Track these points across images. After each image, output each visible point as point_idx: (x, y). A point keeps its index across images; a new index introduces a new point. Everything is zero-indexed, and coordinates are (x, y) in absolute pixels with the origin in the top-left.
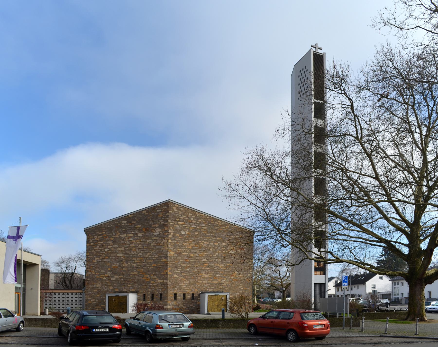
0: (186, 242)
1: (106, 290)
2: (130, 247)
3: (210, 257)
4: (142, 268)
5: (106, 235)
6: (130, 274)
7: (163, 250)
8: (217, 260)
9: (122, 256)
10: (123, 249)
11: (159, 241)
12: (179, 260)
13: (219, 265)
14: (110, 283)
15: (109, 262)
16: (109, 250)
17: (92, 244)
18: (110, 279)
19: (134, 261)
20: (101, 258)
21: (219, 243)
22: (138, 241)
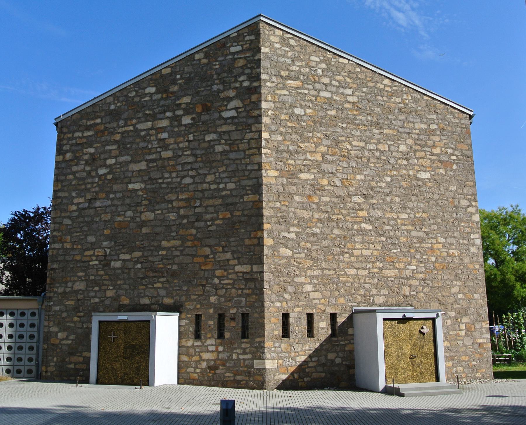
0: (306, 140)
1: (97, 300)
2: (161, 158)
4: (192, 224)
5: (102, 127)
6: (160, 248)
7: (247, 165)
8: (388, 199)
9: (141, 190)
10: (143, 166)
11: (235, 136)
12: (292, 195)
14: (107, 277)
15: (108, 210)
16: (109, 173)
17: (68, 156)
18: (108, 265)
19: (171, 202)
20: (89, 196)
21: (389, 146)
22: (181, 139)
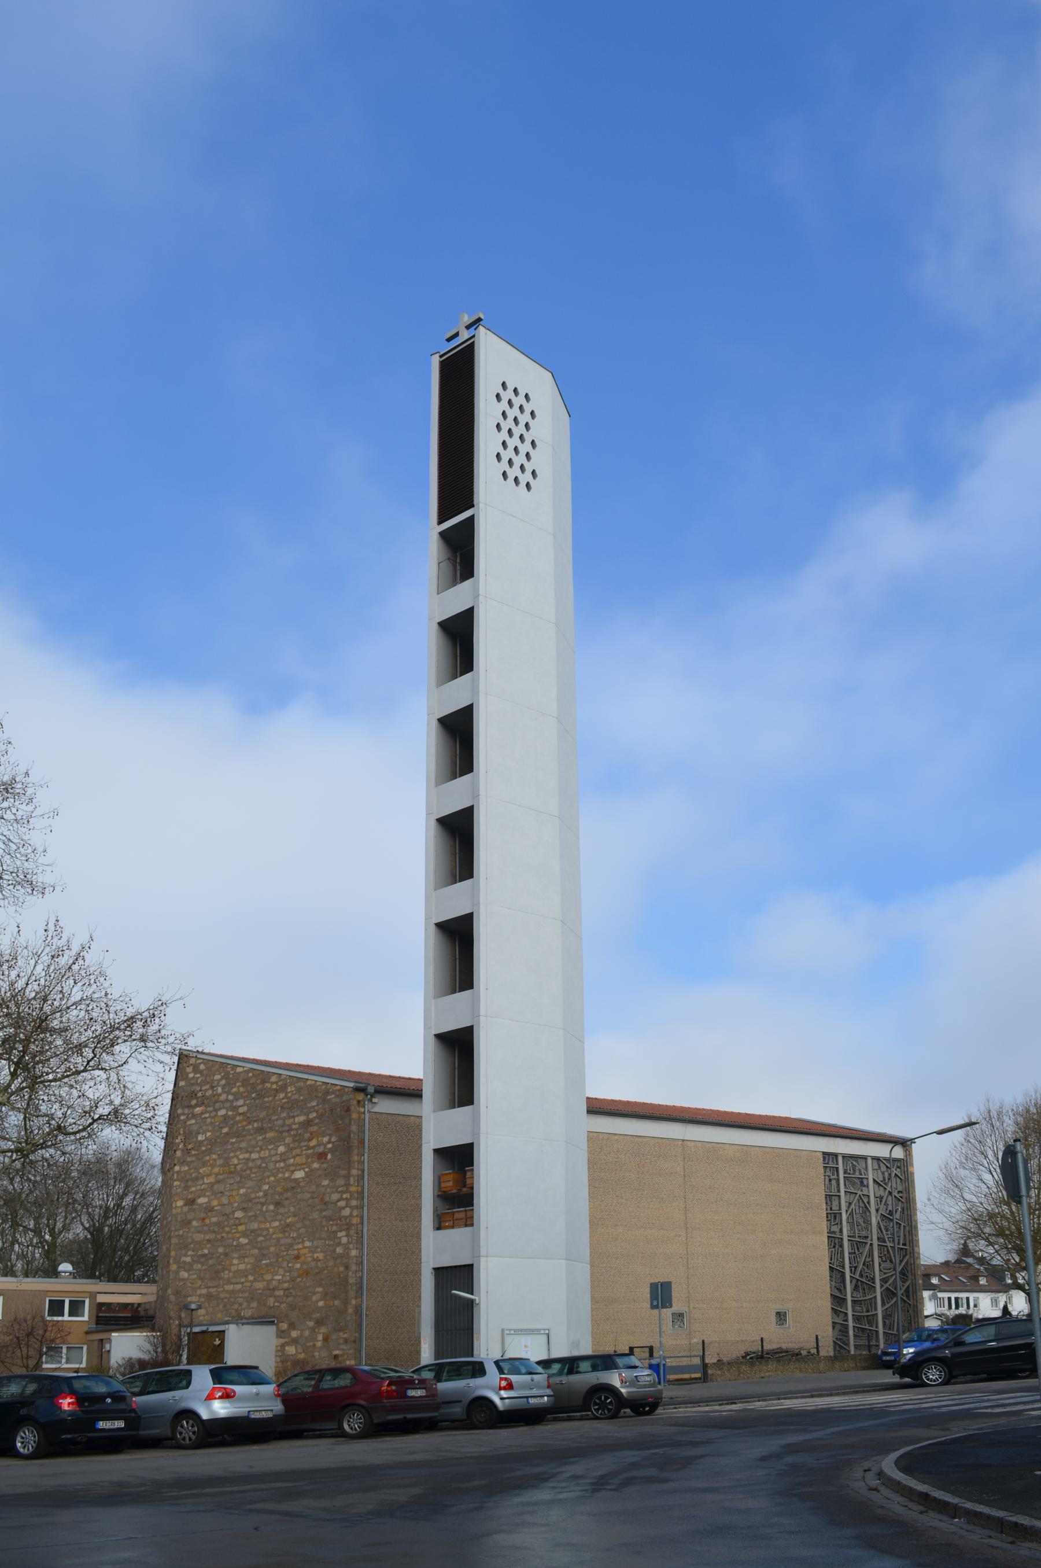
3: (250, 1200)
13: (268, 1225)
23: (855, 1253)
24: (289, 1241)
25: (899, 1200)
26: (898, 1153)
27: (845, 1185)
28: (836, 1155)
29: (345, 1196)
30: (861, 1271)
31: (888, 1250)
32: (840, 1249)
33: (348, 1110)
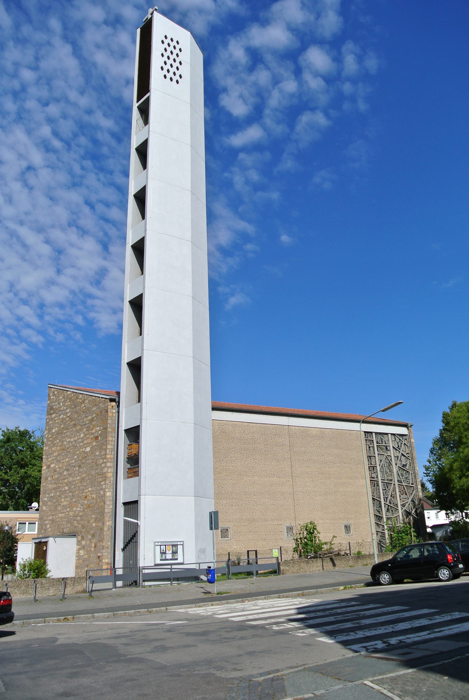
23: (386, 490)
24: (83, 487)
25: (408, 458)
26: (403, 431)
27: (378, 450)
28: (371, 433)
29: (105, 461)
30: (390, 500)
31: (404, 487)
32: (377, 487)
33: (107, 411)
